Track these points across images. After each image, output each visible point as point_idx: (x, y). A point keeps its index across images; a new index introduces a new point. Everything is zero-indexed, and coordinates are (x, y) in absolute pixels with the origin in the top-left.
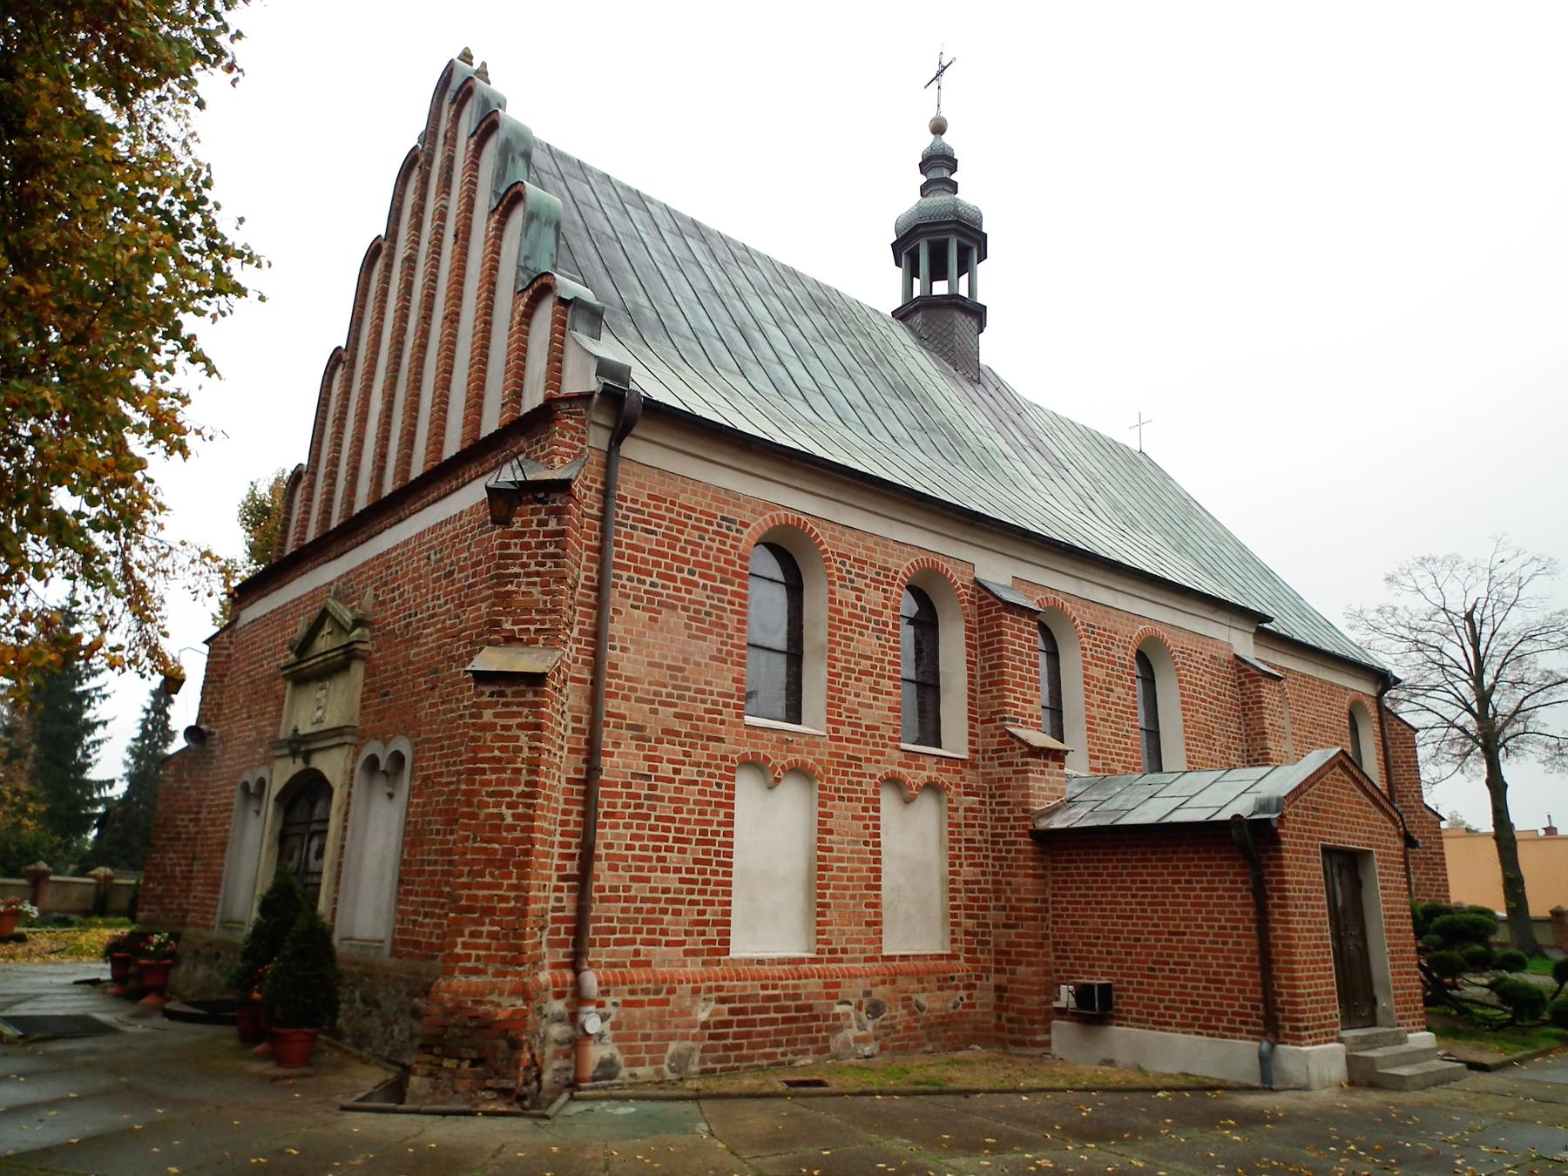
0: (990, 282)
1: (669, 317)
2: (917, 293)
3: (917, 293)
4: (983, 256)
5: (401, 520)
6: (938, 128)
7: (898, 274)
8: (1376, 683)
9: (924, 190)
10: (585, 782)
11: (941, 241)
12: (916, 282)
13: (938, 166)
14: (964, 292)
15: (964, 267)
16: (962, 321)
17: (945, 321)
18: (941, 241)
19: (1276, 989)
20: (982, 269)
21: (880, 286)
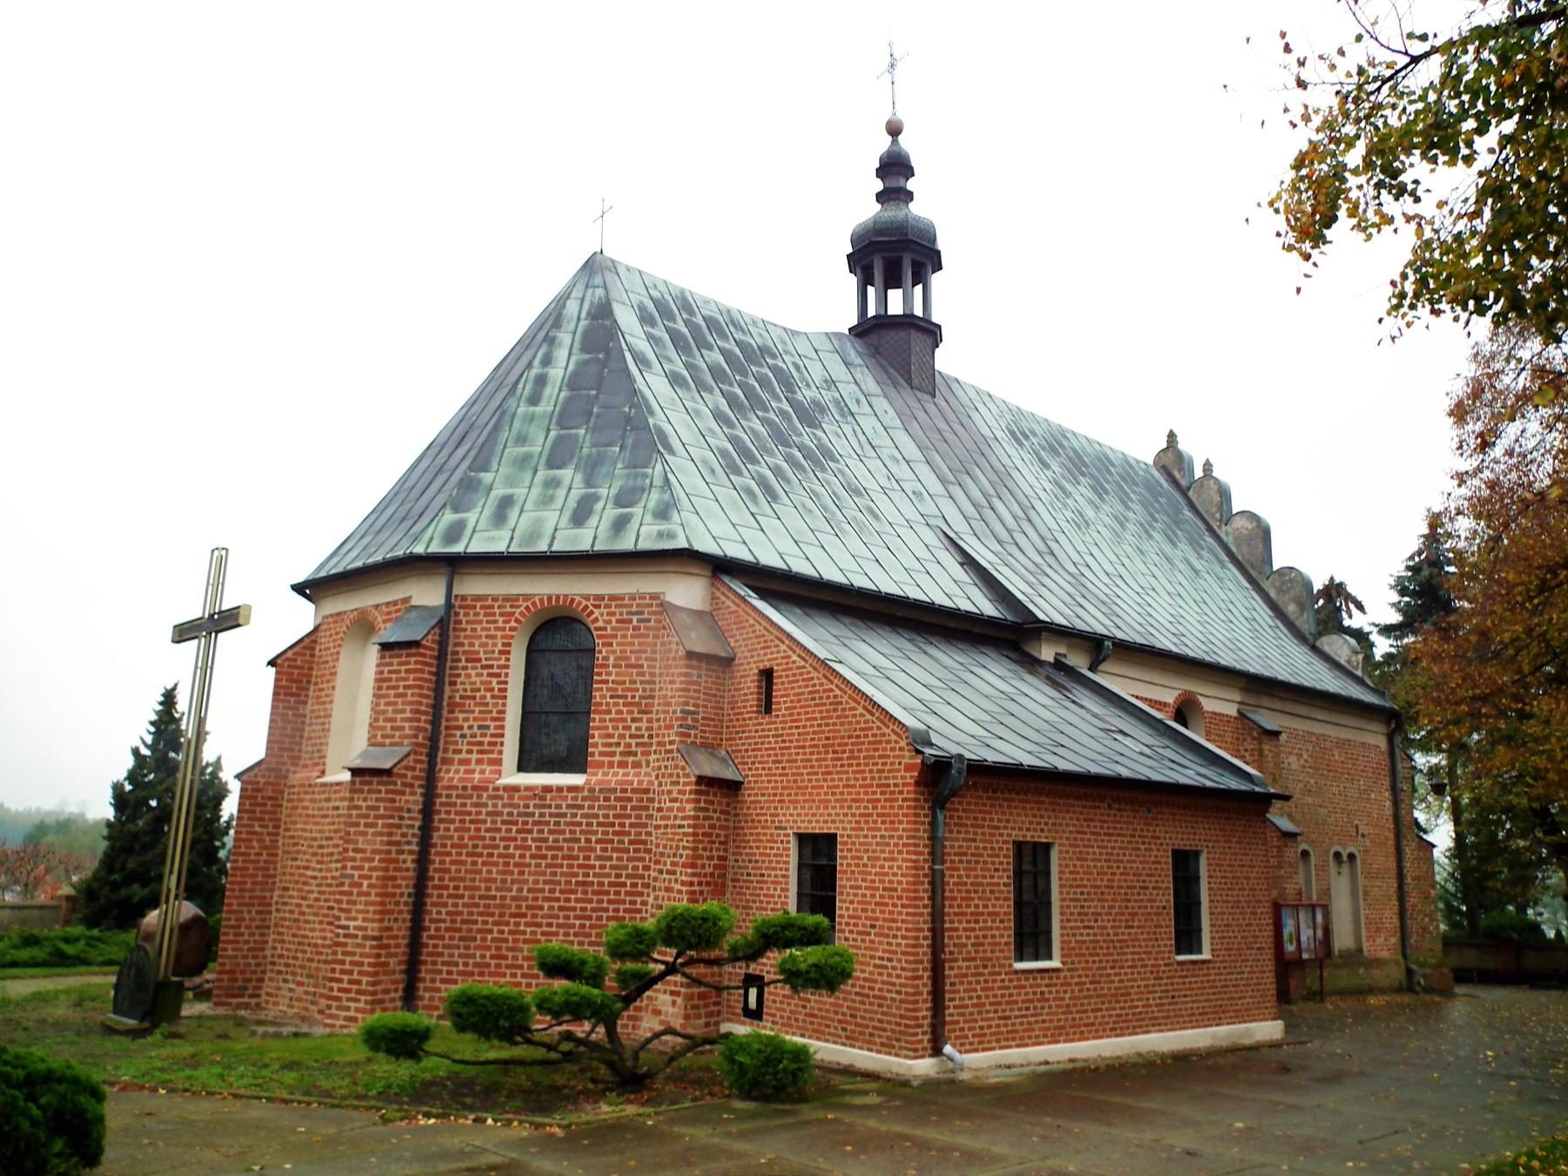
0: (946, 297)
1: (688, 426)
2: (871, 312)
3: (871, 312)
4: (938, 267)
5: (1072, 1061)
6: (894, 130)
7: (852, 281)
8: (1388, 723)
9: (881, 197)
10: (436, 674)
11: (894, 253)
12: (871, 290)
13: (895, 168)
14: (918, 312)
15: (920, 277)
16: (917, 340)
17: (897, 345)
18: (894, 253)
19: (425, 940)
20: (936, 279)
21: (830, 301)
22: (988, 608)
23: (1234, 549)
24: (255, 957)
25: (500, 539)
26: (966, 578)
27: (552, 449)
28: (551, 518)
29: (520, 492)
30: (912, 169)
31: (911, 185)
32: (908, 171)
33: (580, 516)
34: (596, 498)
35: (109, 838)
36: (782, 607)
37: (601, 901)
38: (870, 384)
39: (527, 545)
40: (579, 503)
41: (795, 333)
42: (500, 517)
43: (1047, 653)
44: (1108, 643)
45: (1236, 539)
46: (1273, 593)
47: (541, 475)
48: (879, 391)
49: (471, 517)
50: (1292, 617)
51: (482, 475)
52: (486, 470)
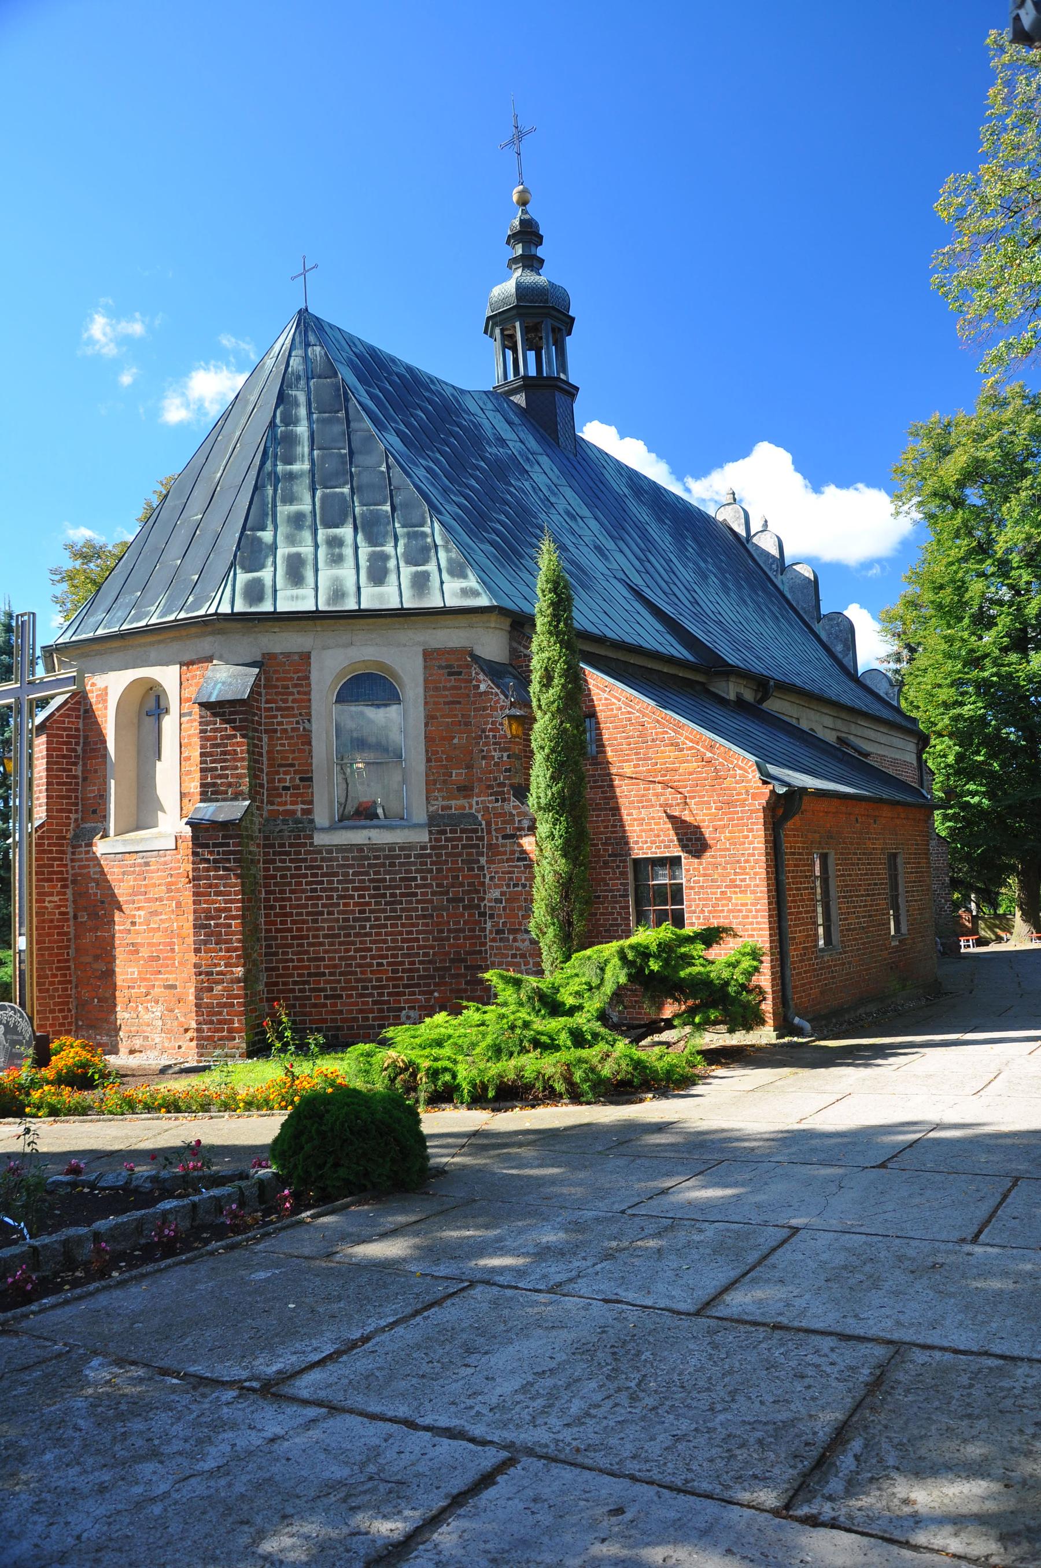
18: (538, 319)
22: (678, 651)
23: (789, 597)
24: (61, 1011)
25: (304, 598)
26: (660, 628)
27: (322, 508)
28: (347, 573)
29: (306, 550)
30: (541, 237)
31: (540, 252)
32: (539, 240)
33: (378, 575)
34: (385, 557)
35: (564, 855)
36: (153, 655)
37: (392, 926)
38: (532, 444)
39: (335, 603)
40: (369, 560)
41: (462, 392)
42: (295, 577)
43: (731, 690)
44: (772, 683)
45: (791, 588)
46: (823, 636)
47: (322, 533)
48: (540, 450)
49: (266, 575)
50: (840, 656)
51: (259, 534)
52: (263, 529)
